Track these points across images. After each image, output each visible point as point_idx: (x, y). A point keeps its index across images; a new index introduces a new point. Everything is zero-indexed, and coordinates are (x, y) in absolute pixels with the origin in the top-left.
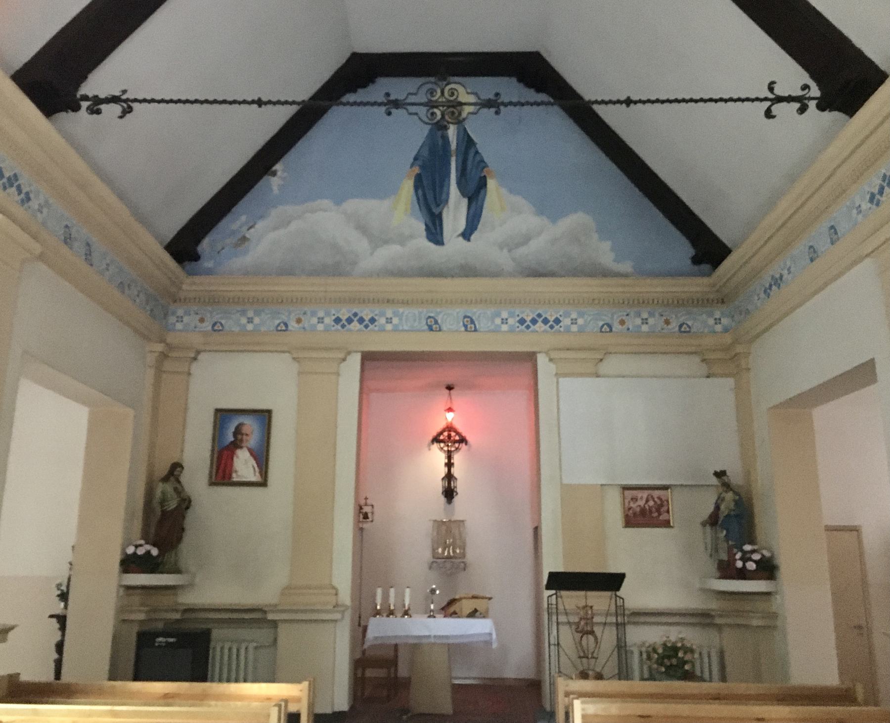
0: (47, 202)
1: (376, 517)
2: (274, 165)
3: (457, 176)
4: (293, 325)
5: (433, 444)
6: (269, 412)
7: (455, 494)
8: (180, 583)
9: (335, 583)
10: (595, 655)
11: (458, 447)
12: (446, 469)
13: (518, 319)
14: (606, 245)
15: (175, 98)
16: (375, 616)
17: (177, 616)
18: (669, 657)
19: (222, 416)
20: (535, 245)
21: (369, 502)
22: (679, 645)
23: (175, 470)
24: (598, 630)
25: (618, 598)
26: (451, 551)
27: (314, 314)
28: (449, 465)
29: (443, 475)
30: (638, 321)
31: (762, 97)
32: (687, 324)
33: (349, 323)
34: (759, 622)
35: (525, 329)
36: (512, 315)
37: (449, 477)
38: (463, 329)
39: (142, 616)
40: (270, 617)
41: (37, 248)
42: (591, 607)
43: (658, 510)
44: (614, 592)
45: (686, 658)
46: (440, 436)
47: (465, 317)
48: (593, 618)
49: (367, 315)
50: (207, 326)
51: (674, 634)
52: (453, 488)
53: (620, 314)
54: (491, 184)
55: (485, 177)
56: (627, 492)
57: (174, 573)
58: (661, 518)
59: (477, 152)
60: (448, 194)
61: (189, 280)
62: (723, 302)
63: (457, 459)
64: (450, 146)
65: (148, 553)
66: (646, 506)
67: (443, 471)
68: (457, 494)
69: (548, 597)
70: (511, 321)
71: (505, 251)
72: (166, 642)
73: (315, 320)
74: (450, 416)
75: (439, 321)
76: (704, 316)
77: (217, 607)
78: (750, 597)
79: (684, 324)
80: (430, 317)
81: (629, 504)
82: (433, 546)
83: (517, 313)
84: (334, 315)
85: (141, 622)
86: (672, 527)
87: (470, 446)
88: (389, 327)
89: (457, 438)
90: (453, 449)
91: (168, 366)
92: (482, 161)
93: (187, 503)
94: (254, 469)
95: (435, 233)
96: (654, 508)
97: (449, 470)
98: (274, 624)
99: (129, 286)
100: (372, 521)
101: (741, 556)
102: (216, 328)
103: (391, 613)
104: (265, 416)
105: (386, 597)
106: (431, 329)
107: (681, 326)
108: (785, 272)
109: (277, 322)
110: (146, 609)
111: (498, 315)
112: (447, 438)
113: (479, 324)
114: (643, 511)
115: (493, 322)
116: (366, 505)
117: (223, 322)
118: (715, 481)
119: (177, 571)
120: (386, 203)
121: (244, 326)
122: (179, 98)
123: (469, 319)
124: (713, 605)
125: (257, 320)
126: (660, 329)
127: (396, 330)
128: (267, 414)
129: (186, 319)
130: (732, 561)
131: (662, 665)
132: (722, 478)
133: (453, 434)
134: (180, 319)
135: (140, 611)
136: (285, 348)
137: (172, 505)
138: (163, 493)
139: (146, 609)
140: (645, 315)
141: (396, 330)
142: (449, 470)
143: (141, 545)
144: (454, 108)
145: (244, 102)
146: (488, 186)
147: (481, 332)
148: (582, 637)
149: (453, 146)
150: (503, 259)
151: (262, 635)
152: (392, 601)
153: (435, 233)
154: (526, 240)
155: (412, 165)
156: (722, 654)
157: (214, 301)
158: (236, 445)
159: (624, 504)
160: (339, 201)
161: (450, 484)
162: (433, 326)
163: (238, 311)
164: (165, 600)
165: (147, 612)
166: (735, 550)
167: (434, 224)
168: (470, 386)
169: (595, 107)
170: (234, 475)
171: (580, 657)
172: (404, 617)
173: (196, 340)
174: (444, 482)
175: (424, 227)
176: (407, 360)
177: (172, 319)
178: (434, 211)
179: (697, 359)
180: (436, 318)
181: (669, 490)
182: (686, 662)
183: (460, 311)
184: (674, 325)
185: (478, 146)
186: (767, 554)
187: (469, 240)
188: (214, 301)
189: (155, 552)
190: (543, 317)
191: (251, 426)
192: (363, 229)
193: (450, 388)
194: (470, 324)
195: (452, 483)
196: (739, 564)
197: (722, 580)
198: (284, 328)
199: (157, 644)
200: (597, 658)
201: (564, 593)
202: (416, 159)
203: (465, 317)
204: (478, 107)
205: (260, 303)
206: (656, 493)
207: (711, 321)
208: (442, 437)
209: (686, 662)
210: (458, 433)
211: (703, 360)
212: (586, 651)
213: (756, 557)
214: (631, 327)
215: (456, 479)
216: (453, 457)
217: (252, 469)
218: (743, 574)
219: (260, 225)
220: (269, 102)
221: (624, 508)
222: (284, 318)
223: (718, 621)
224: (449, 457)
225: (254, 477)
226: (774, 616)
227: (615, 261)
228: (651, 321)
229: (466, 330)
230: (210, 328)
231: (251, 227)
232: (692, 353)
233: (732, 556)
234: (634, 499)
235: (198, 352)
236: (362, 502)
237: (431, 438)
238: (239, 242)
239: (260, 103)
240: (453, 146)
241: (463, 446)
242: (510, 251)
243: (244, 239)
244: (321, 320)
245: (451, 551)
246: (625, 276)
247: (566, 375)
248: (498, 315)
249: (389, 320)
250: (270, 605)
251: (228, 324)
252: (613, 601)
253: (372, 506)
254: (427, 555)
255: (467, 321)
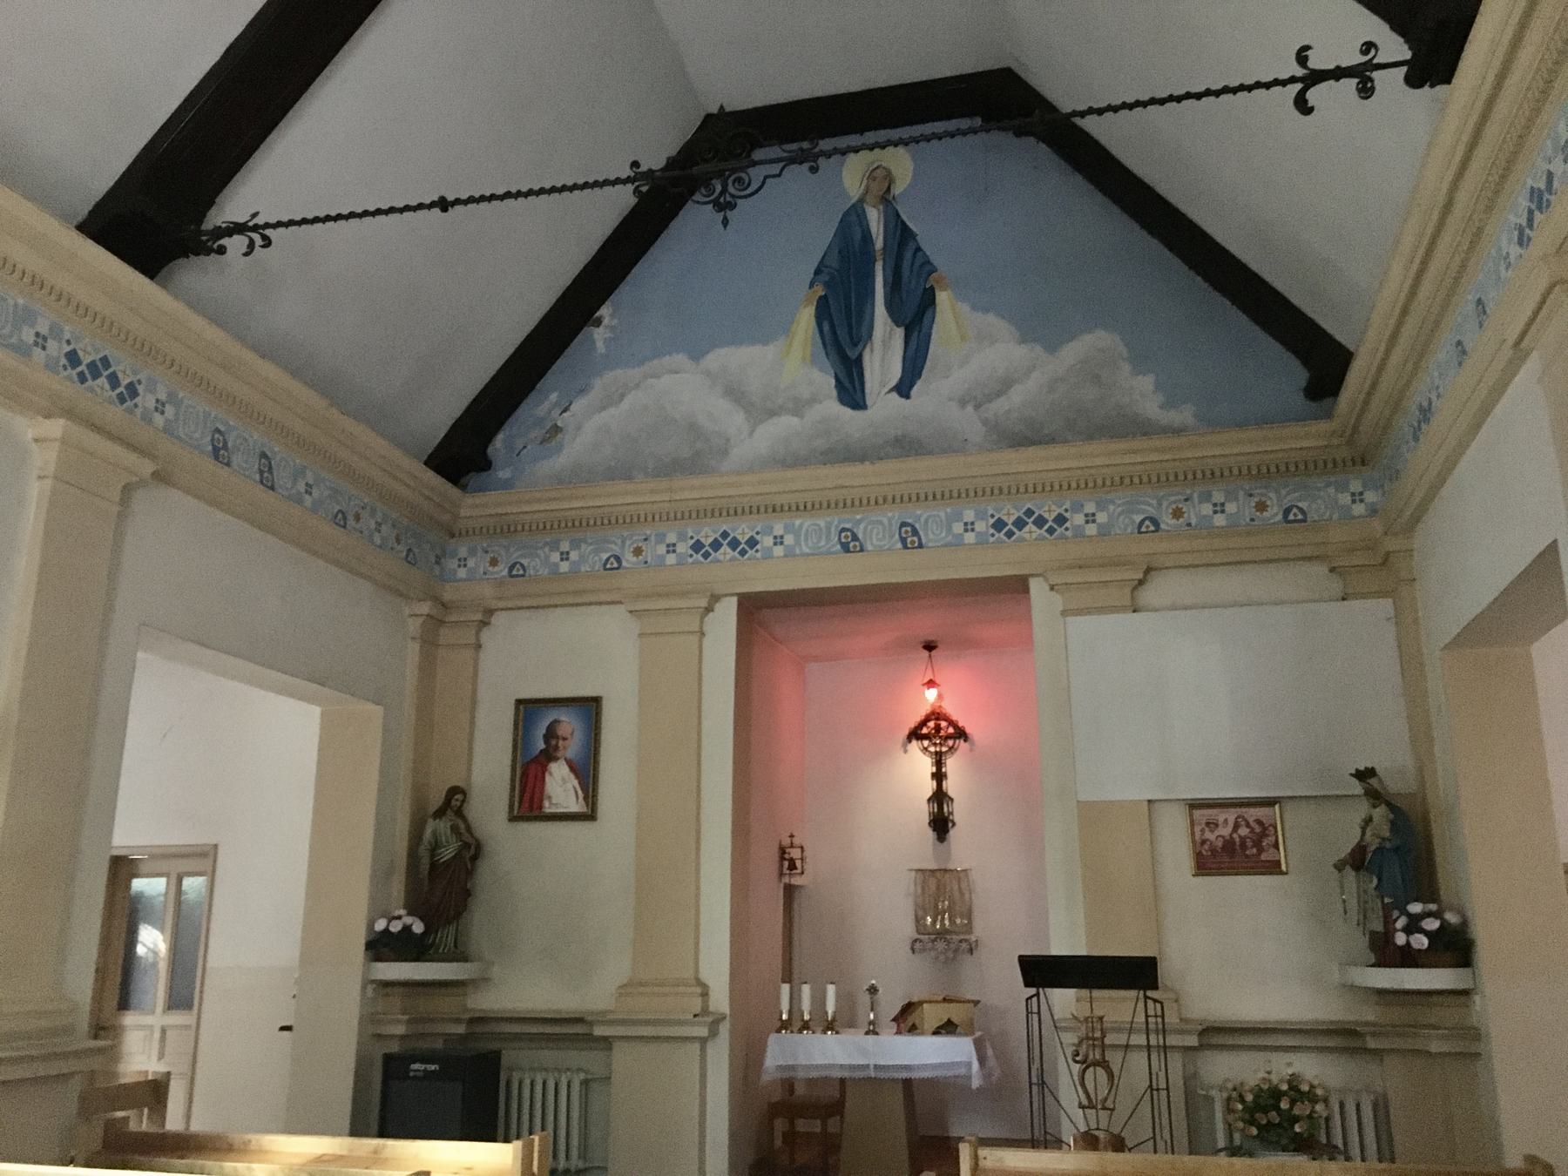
0: (172, 396)
1: (809, 868)
2: (598, 308)
3: (885, 293)
4: (629, 559)
5: (910, 742)
6: (596, 701)
7: (950, 825)
8: (465, 977)
9: (705, 975)
10: (1109, 1104)
11: (953, 745)
12: (935, 783)
13: (992, 521)
14: (1146, 383)
15: (310, 216)
16: (779, 1031)
17: (461, 1029)
18: (1265, 1111)
19: (528, 709)
20: (1016, 397)
21: (796, 841)
22: (1285, 1087)
23: (455, 802)
24: (1115, 1059)
25: (1149, 1002)
26: (947, 922)
27: (661, 538)
28: (939, 776)
29: (930, 794)
30: (1207, 509)
31: (1284, 76)
32: (1298, 507)
33: (716, 550)
34: (1444, 1047)
35: (1005, 538)
36: (981, 515)
37: (939, 797)
38: (899, 545)
39: (400, 1030)
40: (598, 1031)
41: (148, 467)
42: (1101, 1019)
43: (1258, 843)
44: (1142, 992)
45: (1296, 1111)
46: (922, 729)
47: (904, 524)
48: (1103, 1037)
49: (743, 533)
50: (502, 570)
51: (1281, 1067)
52: (946, 815)
53: (1173, 498)
54: (943, 298)
55: (932, 289)
56: (1197, 813)
57: (458, 960)
58: (1264, 857)
59: (918, 249)
60: (871, 327)
61: (469, 500)
62: (1363, 463)
63: (951, 765)
64: (873, 245)
65: (407, 929)
66: (1235, 836)
67: (929, 787)
68: (954, 824)
69: (1027, 999)
70: (980, 526)
71: (970, 408)
72: (425, 1070)
73: (662, 549)
74: (931, 694)
75: (860, 536)
76: (1331, 490)
77: (565, 1016)
78: (1434, 998)
79: (515, 564)
80: (843, 530)
81: (1202, 835)
82: (916, 916)
83: (990, 512)
84: (692, 538)
85: (402, 1037)
86: (1282, 873)
87: (973, 744)
88: (779, 551)
89: (951, 730)
90: (944, 749)
91: (446, 635)
92: (928, 262)
93: (472, 851)
94: (576, 792)
95: (851, 391)
96: (1248, 840)
97: (939, 785)
98: (607, 1043)
99: (357, 518)
100: (803, 873)
101: (1405, 923)
102: (514, 572)
103: (806, 1026)
104: (590, 708)
105: (795, 998)
106: (846, 548)
107: (1287, 511)
108: (1434, 398)
109: (605, 556)
110: (407, 1017)
111: (958, 516)
112: (933, 731)
113: (926, 535)
114: (1229, 845)
115: (949, 529)
116: (792, 846)
117: (525, 562)
118: (1357, 788)
119: (463, 958)
120: (770, 352)
121: (557, 565)
122: (338, 212)
123: (909, 529)
124: (1369, 1014)
125: (574, 555)
126: (1248, 520)
127: (789, 554)
128: (595, 704)
129: (471, 563)
130: (1388, 934)
131: (1251, 1124)
132: (1368, 781)
133: (943, 724)
134: (463, 562)
135: (399, 1021)
136: (615, 597)
137: (447, 853)
138: (434, 833)
139: (407, 1017)
140: (1218, 497)
141: (789, 554)
142: (939, 785)
143: (399, 918)
144: (742, 172)
145: (420, 206)
146: (937, 301)
147: (928, 547)
148: (1084, 1071)
149: (879, 244)
150: (968, 423)
151: (588, 1060)
152: (806, 1005)
153: (851, 391)
154: (1004, 386)
155: (811, 285)
156: (1381, 1107)
157: (506, 530)
158: (549, 755)
159: (1193, 834)
160: (697, 356)
161: (943, 809)
162: (850, 543)
163: (546, 544)
164: (445, 1004)
165: (409, 1022)
166: (1396, 913)
167: (850, 375)
168: (965, 644)
169: (1090, 124)
170: (546, 804)
171: (1081, 1106)
172: (780, 1032)
173: (487, 591)
174: (931, 805)
175: (833, 382)
176: (785, 606)
177: (452, 564)
178: (849, 354)
179: (1321, 569)
180: (855, 530)
181: (1277, 807)
182: (1296, 1119)
183: (893, 515)
184: (1274, 513)
185: (918, 238)
186: (1451, 918)
187: (907, 397)
188: (506, 530)
189: (418, 927)
190: (1036, 515)
191: (570, 724)
192: (735, 394)
193: (930, 647)
194: (910, 537)
195: (945, 806)
196: (1401, 939)
197: (1382, 970)
198: (616, 565)
199: (412, 1074)
200: (1113, 1110)
201: (1097, 993)
202: (818, 272)
203: (904, 524)
204: (782, 164)
205: (577, 526)
206: (1253, 814)
207: (1345, 499)
208: (925, 731)
209: (1296, 1119)
210: (951, 723)
211: (1332, 570)
212: (1093, 1096)
213: (1432, 925)
214: (1194, 522)
215: (952, 800)
216: (945, 763)
217: (573, 792)
218: (1408, 958)
219: (578, 406)
220: (457, 202)
221: (1194, 841)
222: (616, 549)
223: (1372, 1044)
224: (939, 763)
225: (574, 805)
226: (1475, 1034)
227: (1161, 407)
228: (1231, 508)
229: (905, 547)
230: (505, 572)
231: (565, 411)
232: (1310, 559)
233: (1389, 922)
234: (1212, 825)
235: (490, 612)
236: (786, 842)
237: (906, 732)
238: (548, 435)
239: (443, 204)
240: (879, 244)
241: (961, 744)
242: (977, 407)
243: (556, 429)
244: (671, 548)
245: (947, 922)
246: (1177, 431)
247: (1079, 612)
248: (958, 516)
249: (778, 541)
250: (598, 1013)
251: (534, 565)
252: (1141, 1005)
253: (802, 848)
254: (908, 929)
255: (906, 532)
